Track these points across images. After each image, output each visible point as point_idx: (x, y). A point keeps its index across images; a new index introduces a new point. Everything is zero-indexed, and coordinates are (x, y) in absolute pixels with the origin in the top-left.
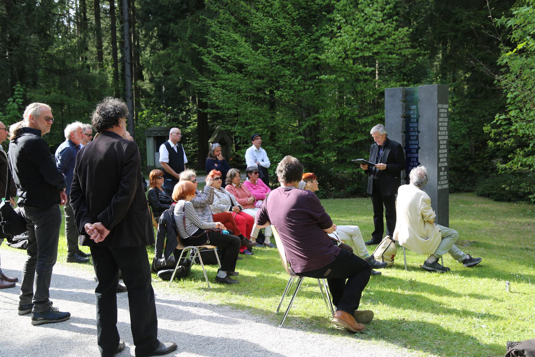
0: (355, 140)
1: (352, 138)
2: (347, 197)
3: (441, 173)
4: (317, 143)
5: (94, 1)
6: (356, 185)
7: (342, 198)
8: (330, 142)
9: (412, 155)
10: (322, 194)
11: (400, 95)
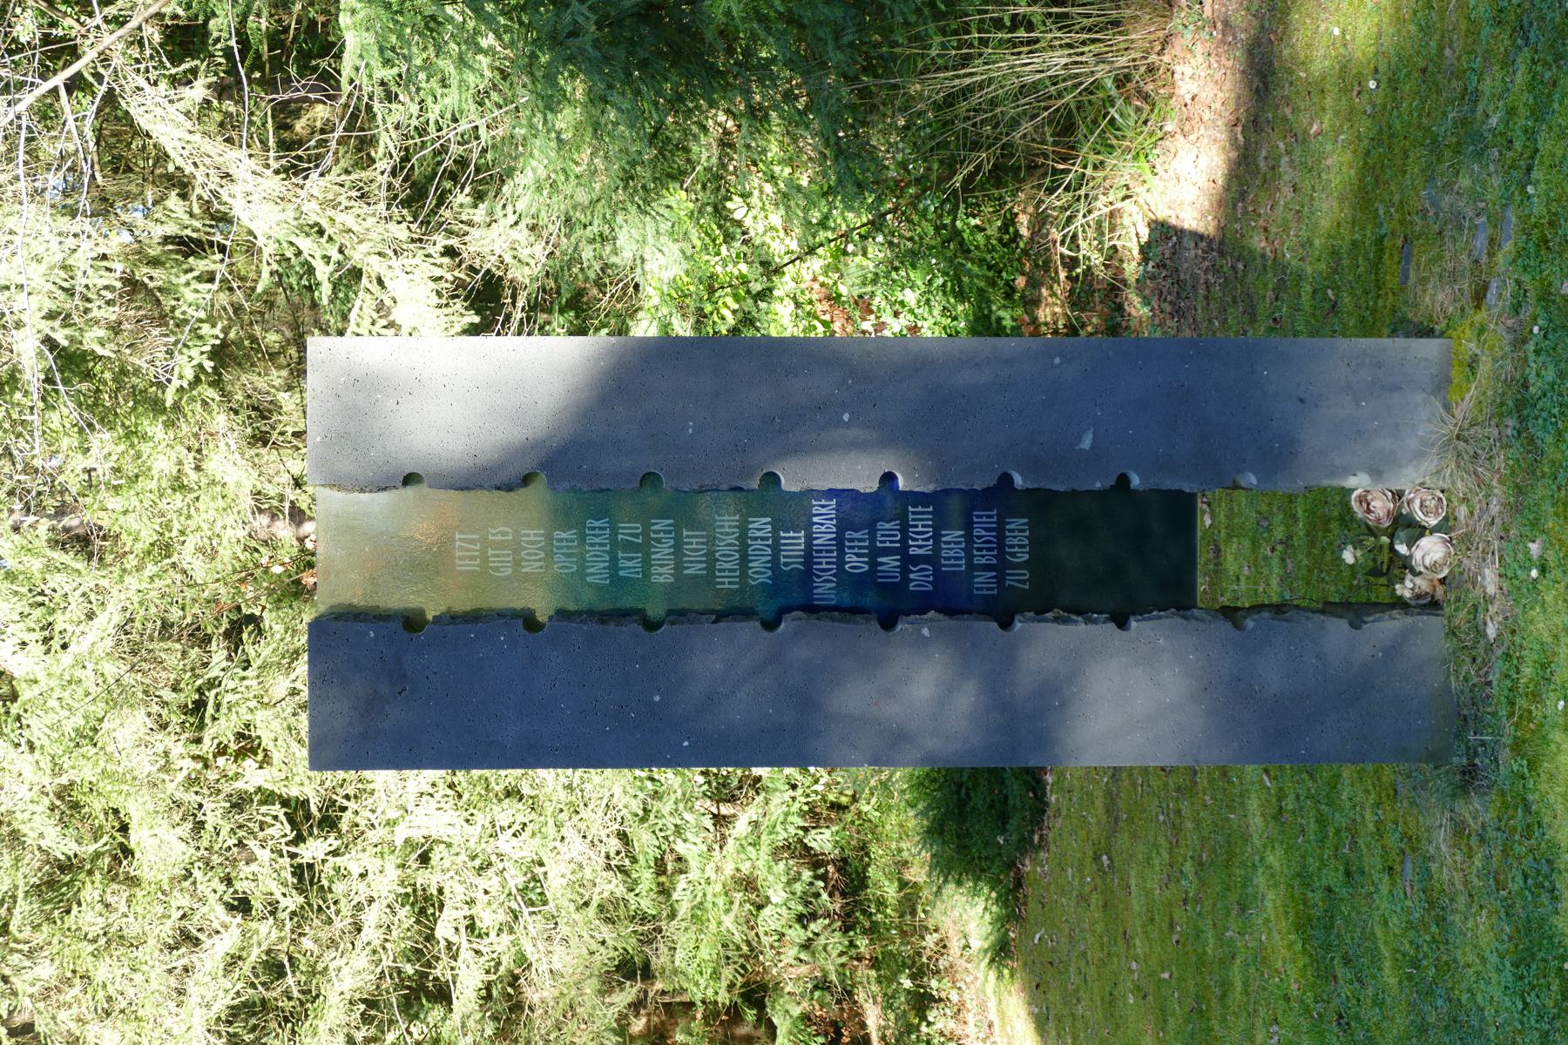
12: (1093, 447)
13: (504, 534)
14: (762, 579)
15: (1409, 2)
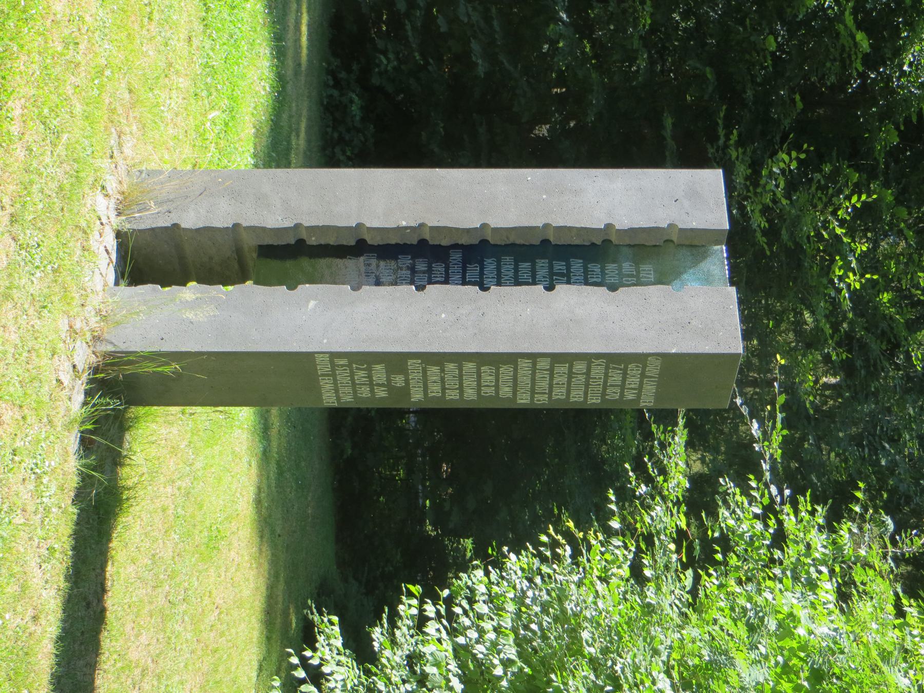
12: (308, 302)
14: (490, 261)
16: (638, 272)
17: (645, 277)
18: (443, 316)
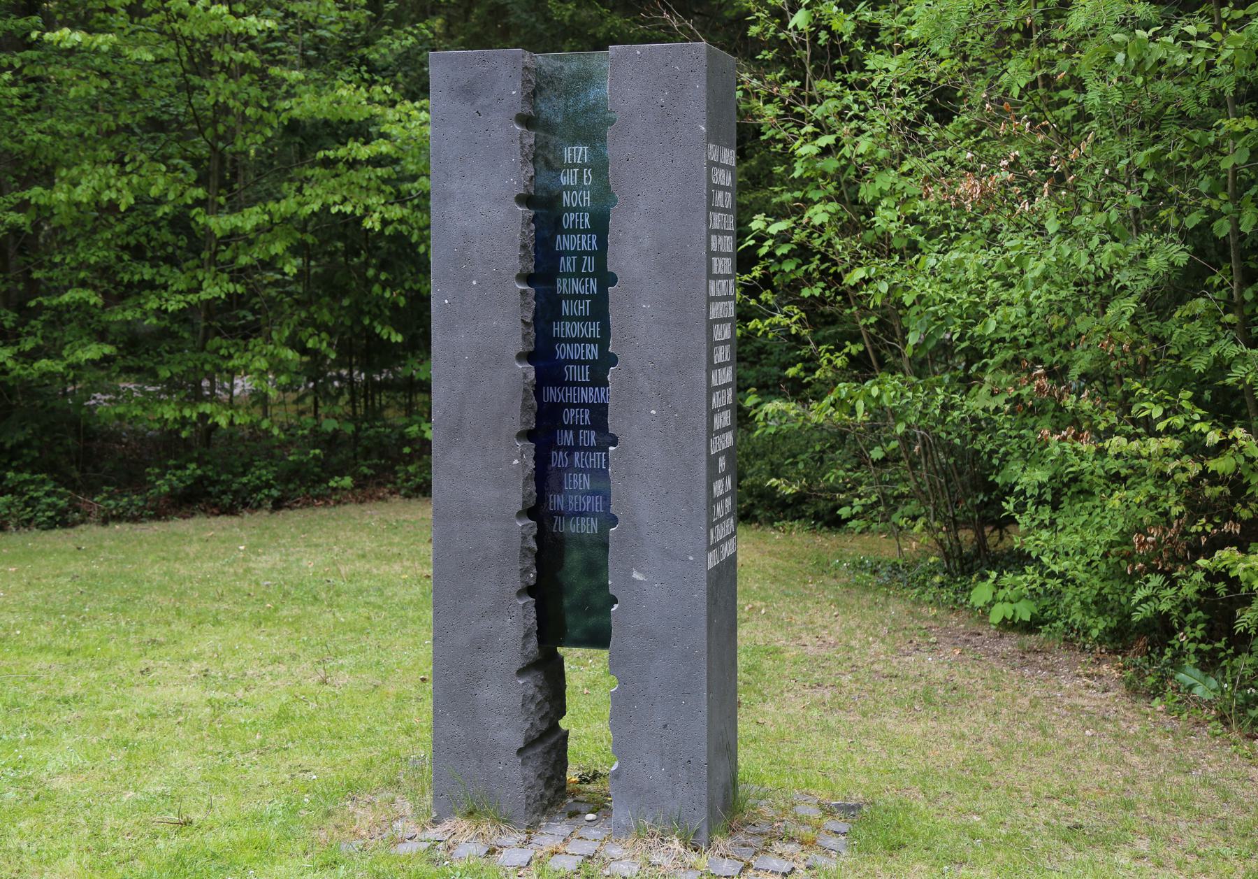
0: (193, 298)
1: (182, 286)
2: (159, 514)
3: (719, 488)
4: (32, 304)
5: (1, 276)
6: (193, 466)
7: (135, 519)
8: (92, 302)
9: (571, 395)
10: (51, 506)
11: (513, 92)
12: (635, 580)
13: (588, 179)
14: (559, 352)
15: (16, 540)
16: (574, 165)
17: (583, 156)
18: (653, 412)
